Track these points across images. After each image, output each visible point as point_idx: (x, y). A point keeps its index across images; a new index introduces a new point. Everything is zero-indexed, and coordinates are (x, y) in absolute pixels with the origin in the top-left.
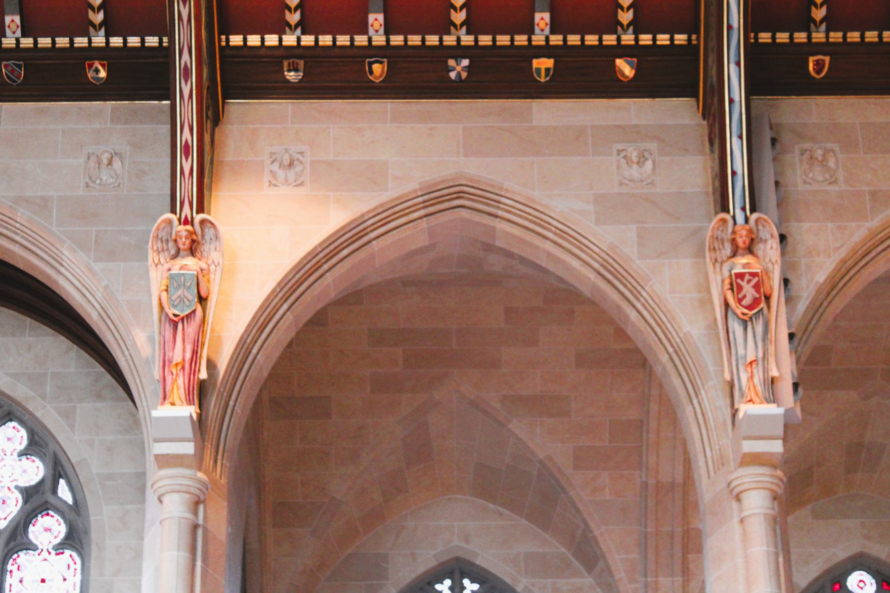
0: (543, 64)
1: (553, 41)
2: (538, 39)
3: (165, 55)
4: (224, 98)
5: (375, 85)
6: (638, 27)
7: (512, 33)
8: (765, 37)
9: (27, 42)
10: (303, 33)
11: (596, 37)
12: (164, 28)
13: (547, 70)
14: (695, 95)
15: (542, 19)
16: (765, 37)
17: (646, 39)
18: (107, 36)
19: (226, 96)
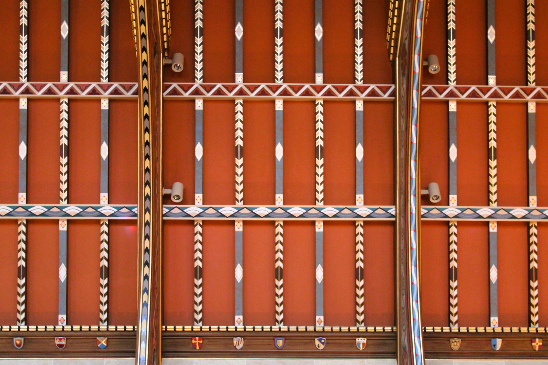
0: (361, 341)
1: (177, 329)
2: (319, 328)
3: (134, 335)
4: (162, 357)
5: (238, 350)
6: (459, 323)
7: (306, 325)
8: (429, 329)
9: (328, 329)
10: (539, 326)
11: (382, 328)
12: (135, 322)
13: (363, 344)
14: (396, 358)
15: (494, 320)
16: (130, 328)
17: (371, 329)
18: (459, 327)
19: (162, 357)
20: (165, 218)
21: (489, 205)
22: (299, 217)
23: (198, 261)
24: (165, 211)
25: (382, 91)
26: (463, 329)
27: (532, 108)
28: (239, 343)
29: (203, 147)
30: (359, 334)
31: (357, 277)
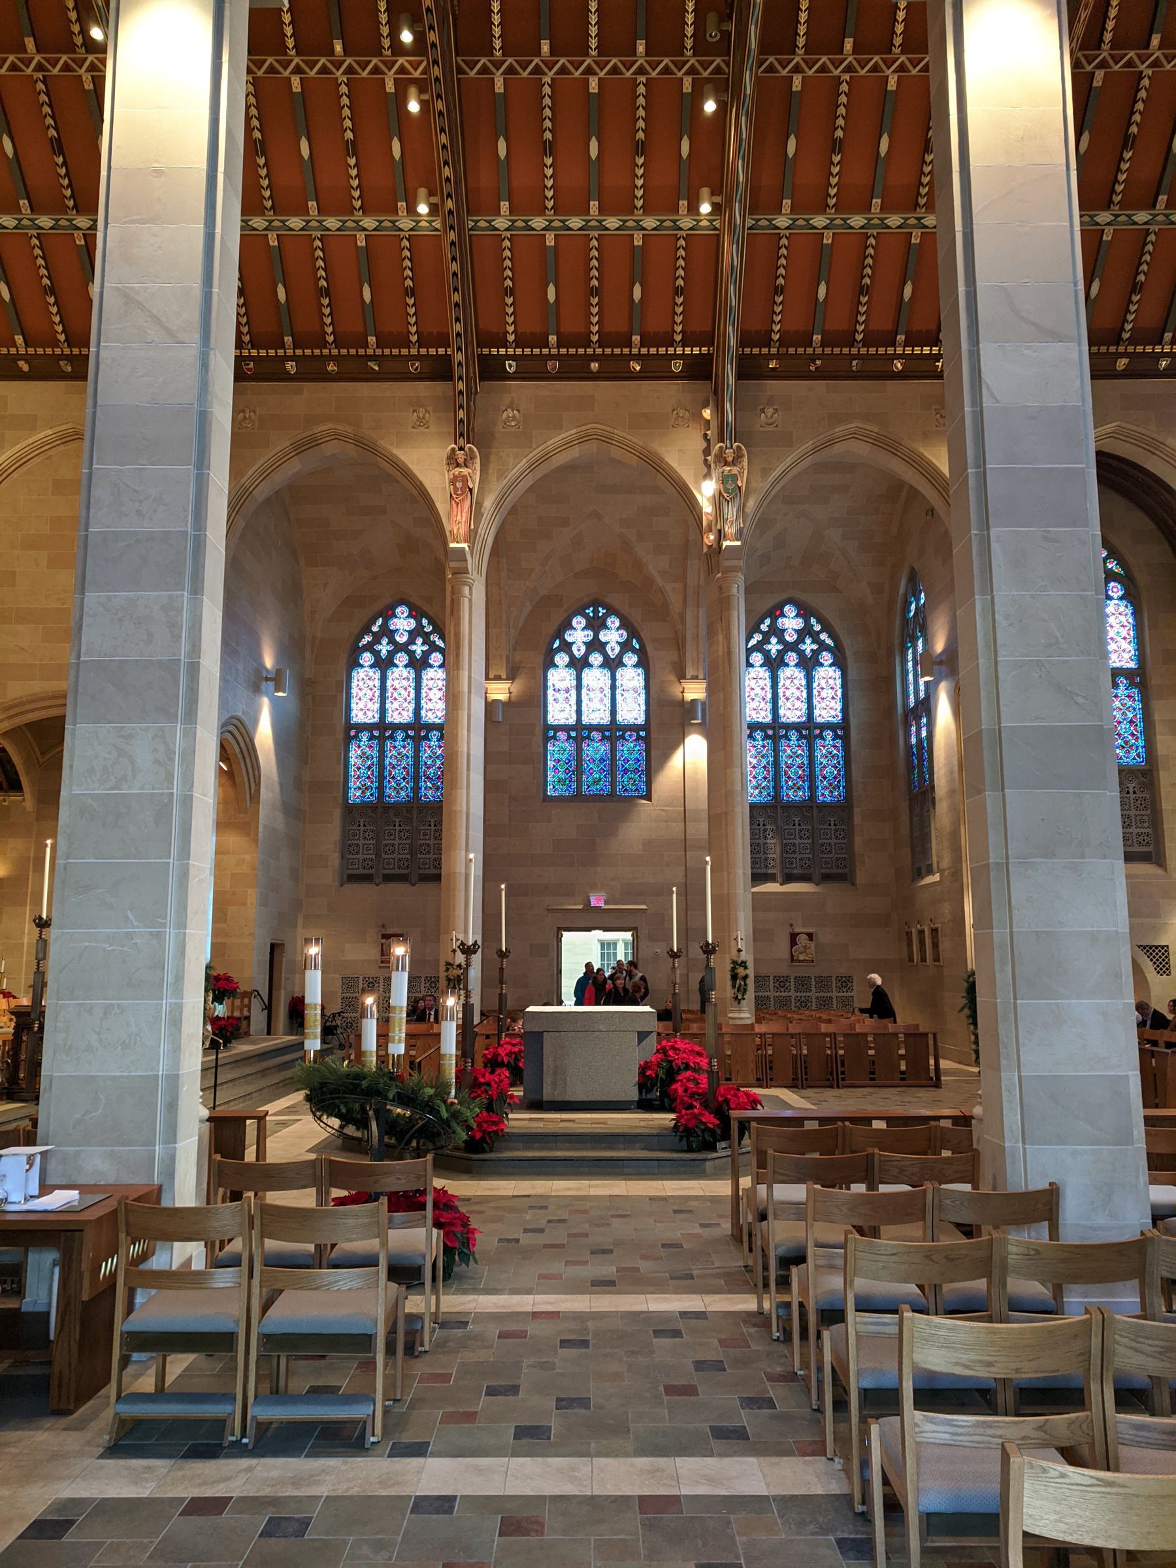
0: (594, 366)
2: (635, 351)
17: (688, 351)
20: (471, 232)
21: (1109, 207)
22: (652, 230)
23: (594, 280)
24: (471, 224)
25: (676, 66)
26: (423, 351)
27: (892, 85)
28: (511, 367)
29: (598, 142)
30: (675, 356)
31: (776, 293)
